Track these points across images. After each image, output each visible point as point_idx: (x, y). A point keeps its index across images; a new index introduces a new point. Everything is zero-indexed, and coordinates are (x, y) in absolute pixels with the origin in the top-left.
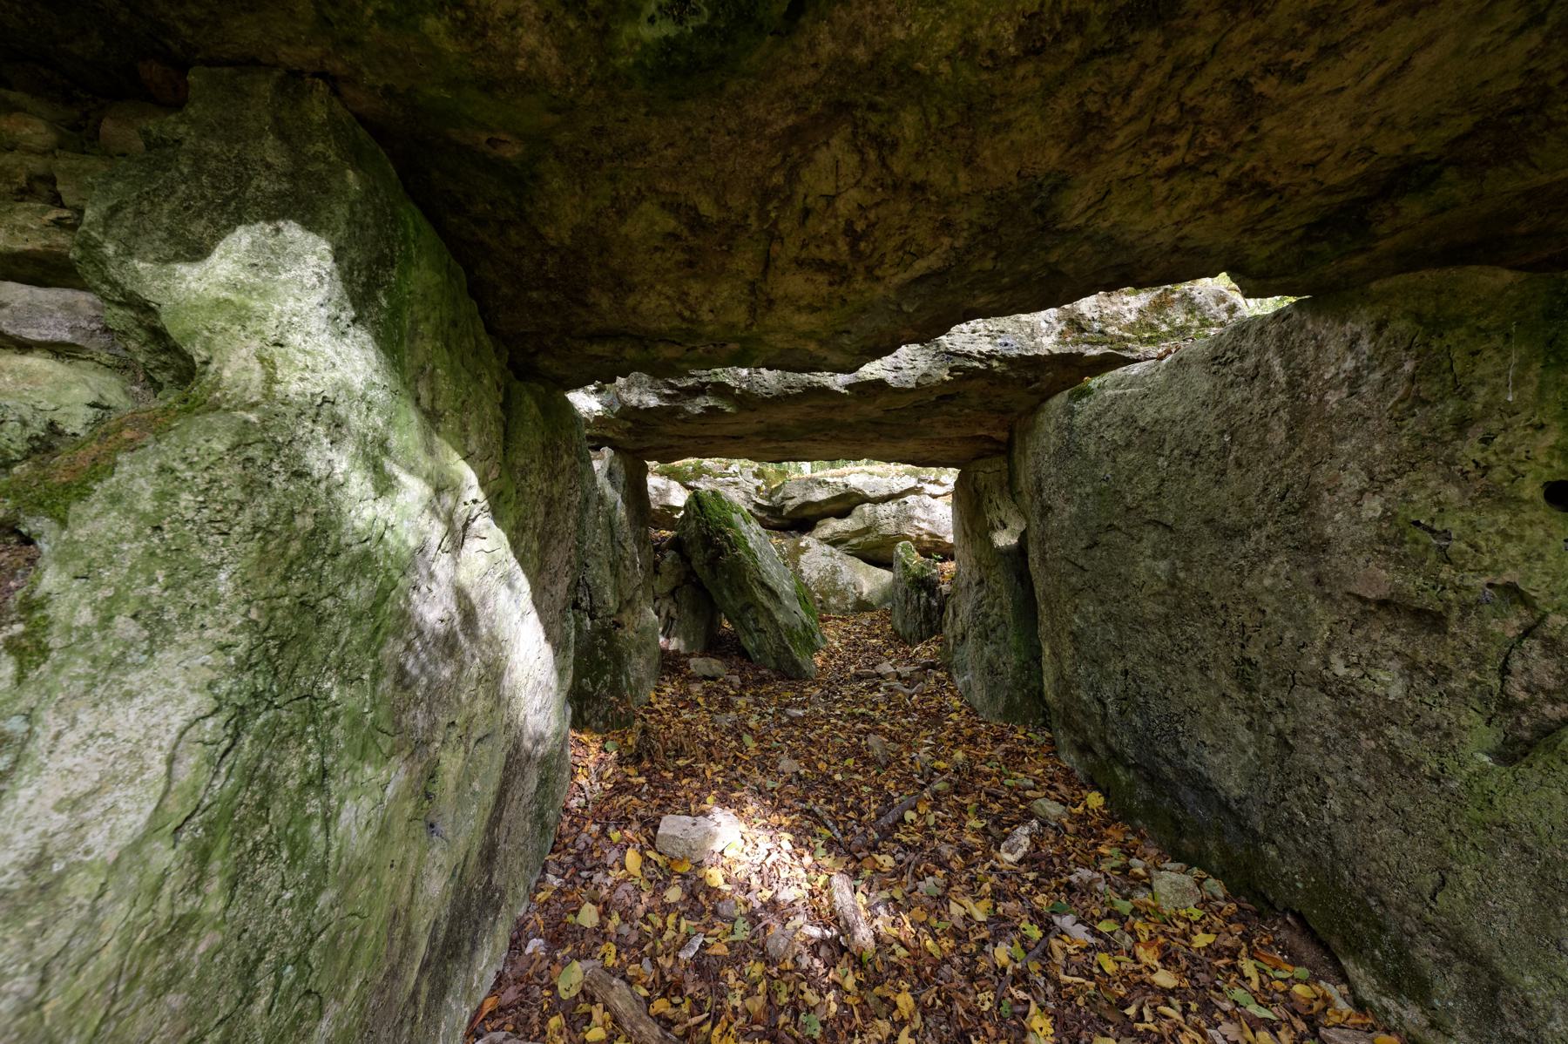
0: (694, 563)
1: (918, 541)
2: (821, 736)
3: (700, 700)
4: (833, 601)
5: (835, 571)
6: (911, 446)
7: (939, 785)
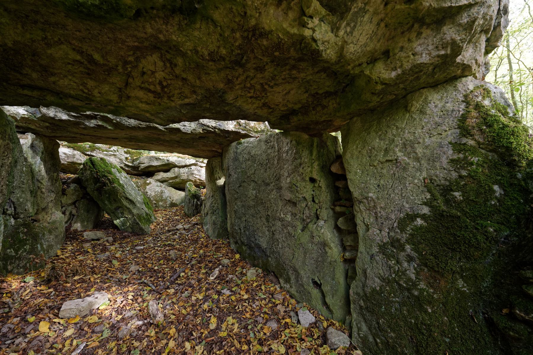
0: (88, 190)
1: (195, 181)
2: (150, 255)
3: (89, 250)
4: (161, 203)
5: (162, 192)
6: (191, 150)
7: (194, 262)
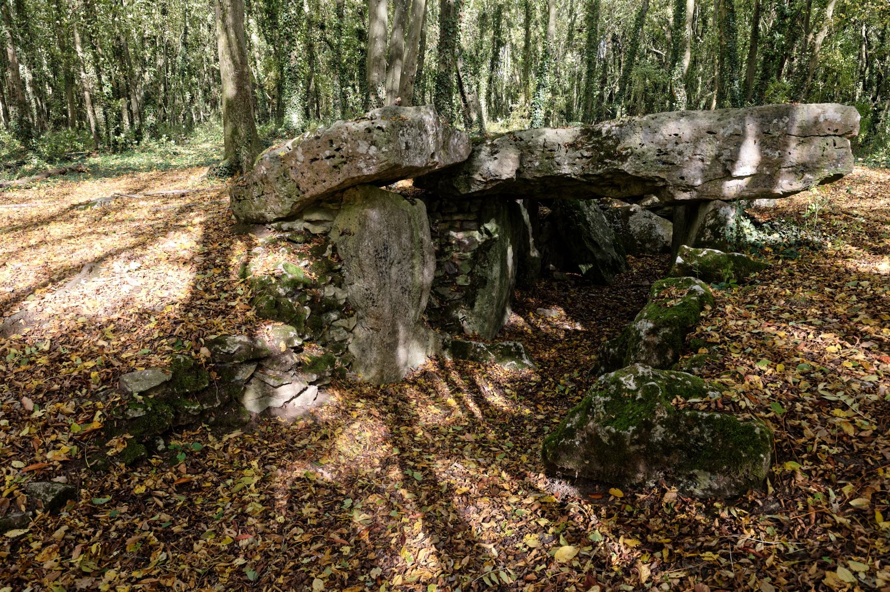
4: (648, 246)
